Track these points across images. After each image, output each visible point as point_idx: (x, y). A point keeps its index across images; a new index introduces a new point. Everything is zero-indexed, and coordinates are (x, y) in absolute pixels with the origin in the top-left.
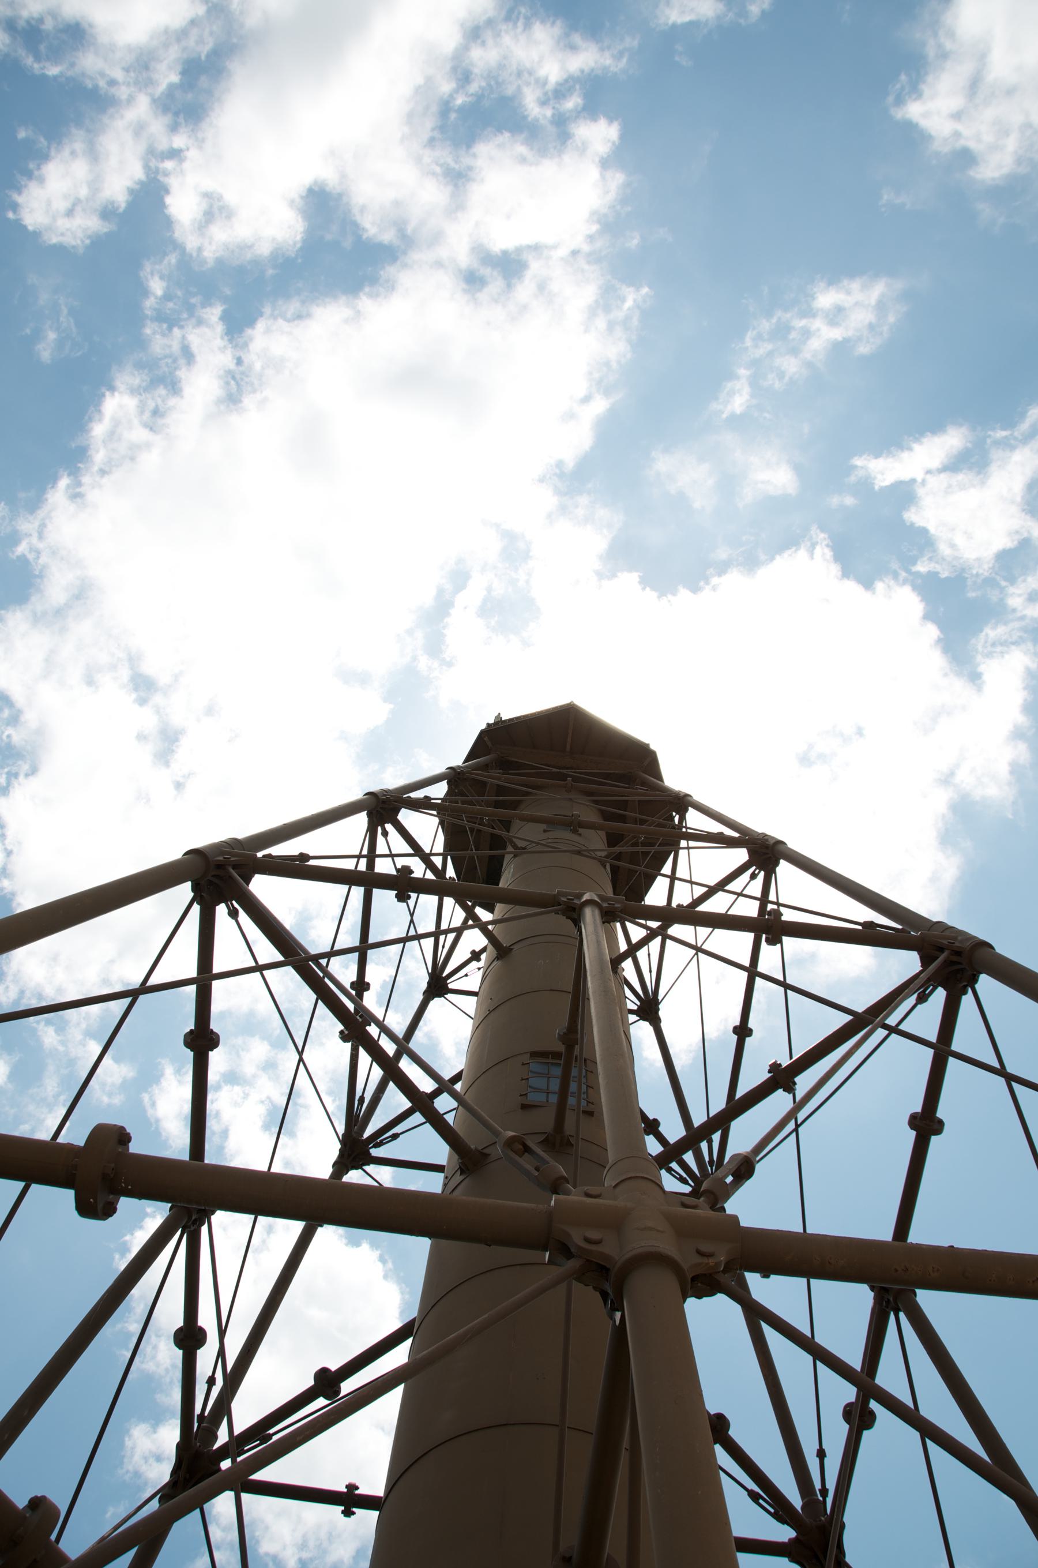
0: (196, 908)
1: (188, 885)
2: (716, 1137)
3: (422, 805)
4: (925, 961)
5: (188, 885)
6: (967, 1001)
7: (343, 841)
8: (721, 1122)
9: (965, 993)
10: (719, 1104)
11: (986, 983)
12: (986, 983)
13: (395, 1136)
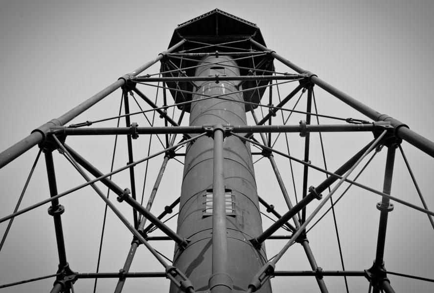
0: (43, 155)
1: (119, 278)
2: (301, 212)
3: (147, 79)
4: (376, 136)
5: (119, 278)
6: (398, 150)
7: (108, 112)
8: (302, 206)
9: (397, 148)
10: (300, 198)
11: (405, 144)
12: (405, 144)
13: (348, 120)
